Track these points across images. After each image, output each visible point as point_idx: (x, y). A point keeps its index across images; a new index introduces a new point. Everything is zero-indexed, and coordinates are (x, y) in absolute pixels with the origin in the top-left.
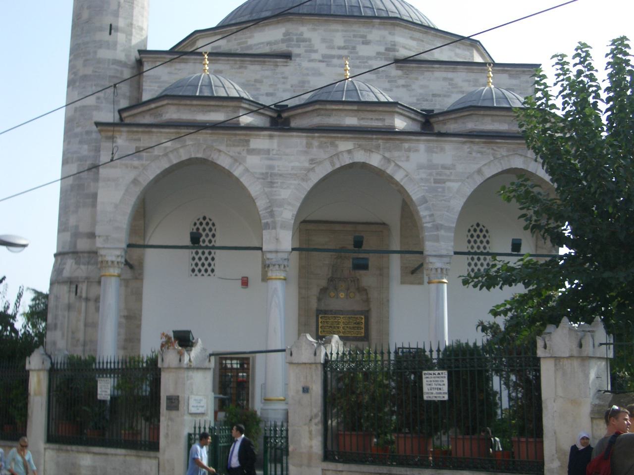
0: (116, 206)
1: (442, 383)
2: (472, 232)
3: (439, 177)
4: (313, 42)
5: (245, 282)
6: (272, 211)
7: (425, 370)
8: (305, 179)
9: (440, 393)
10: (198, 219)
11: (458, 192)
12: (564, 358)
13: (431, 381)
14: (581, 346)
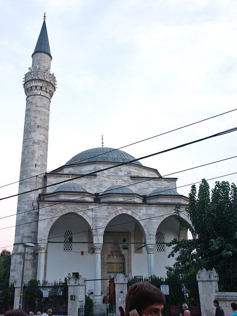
0: (44, 228)
5: (82, 253)
8: (107, 219)
11: (156, 224)
12: (205, 281)
14: (210, 277)
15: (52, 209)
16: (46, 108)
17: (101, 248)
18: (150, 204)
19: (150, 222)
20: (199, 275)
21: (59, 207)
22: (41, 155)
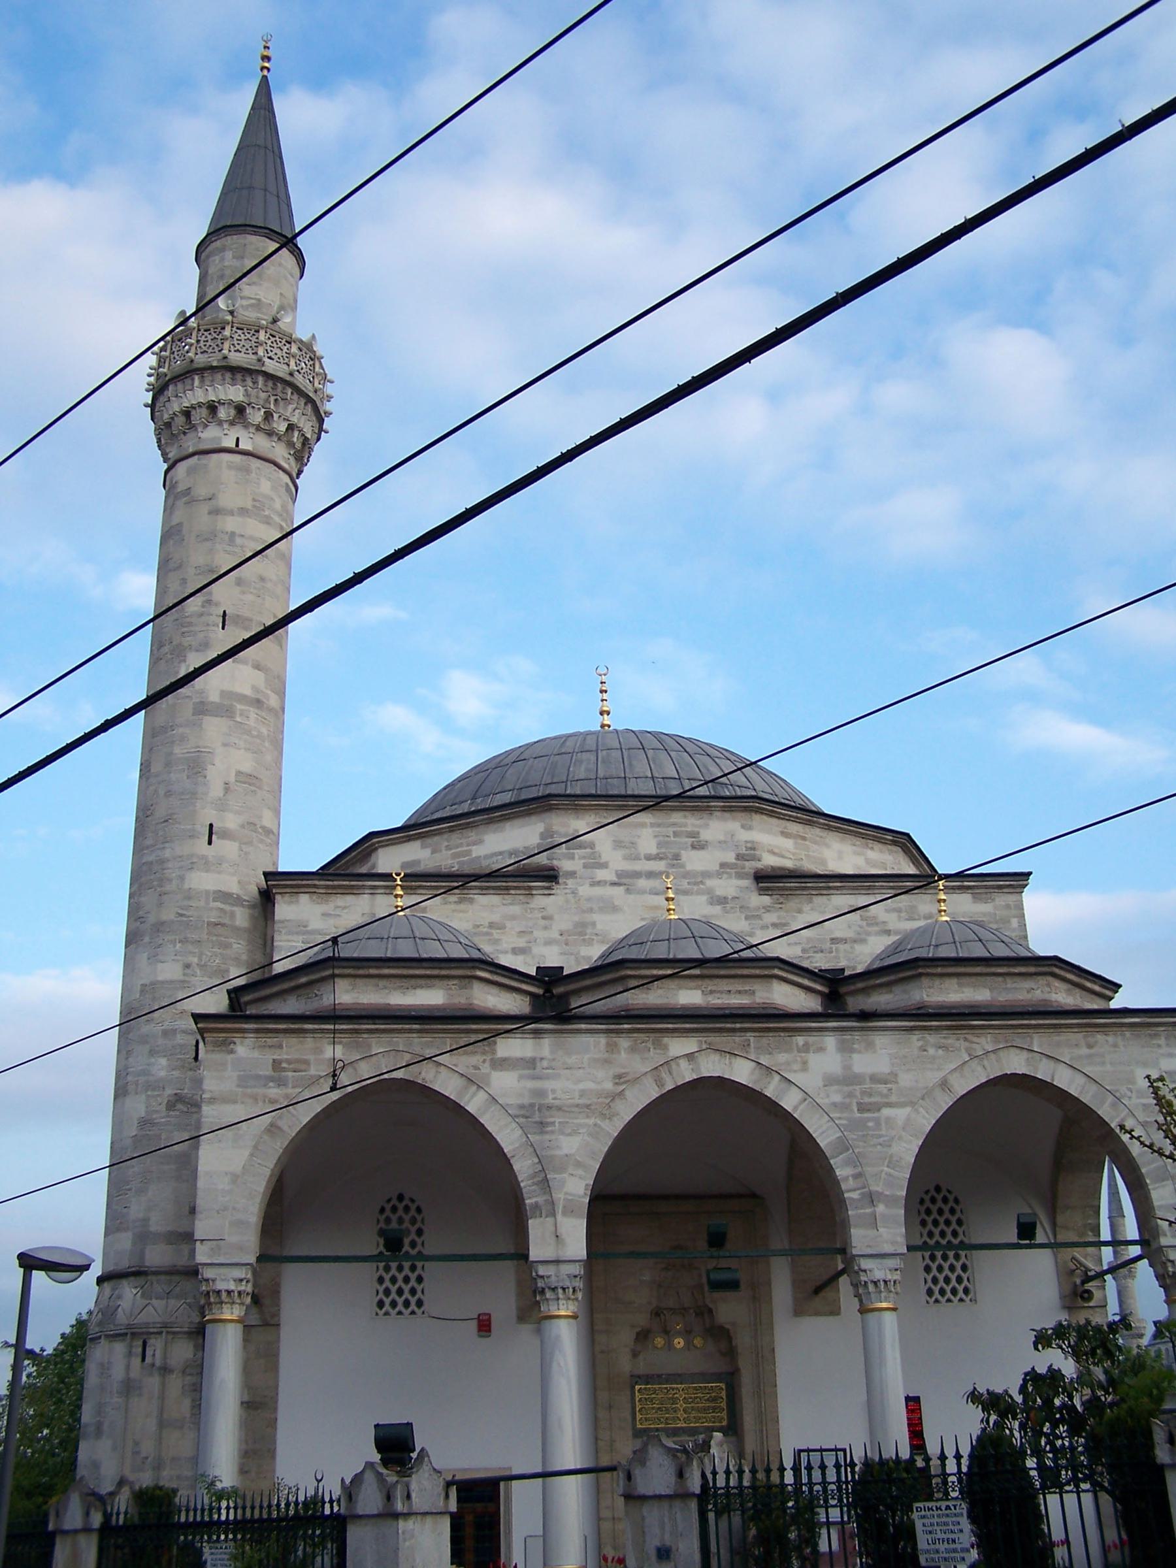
0: (235, 1178)
1: (956, 1528)
2: (928, 1204)
3: (867, 1100)
4: (597, 848)
5: (484, 1325)
6: (546, 1179)
7: (920, 1501)
9: (955, 1551)
10: (389, 1201)
13: (932, 1525)
15: (276, 1065)
16: (268, 517)
17: (579, 1284)
18: (865, 1015)
19: (869, 1120)
20: (1166, 1423)
21: (319, 1051)
22: (239, 773)
